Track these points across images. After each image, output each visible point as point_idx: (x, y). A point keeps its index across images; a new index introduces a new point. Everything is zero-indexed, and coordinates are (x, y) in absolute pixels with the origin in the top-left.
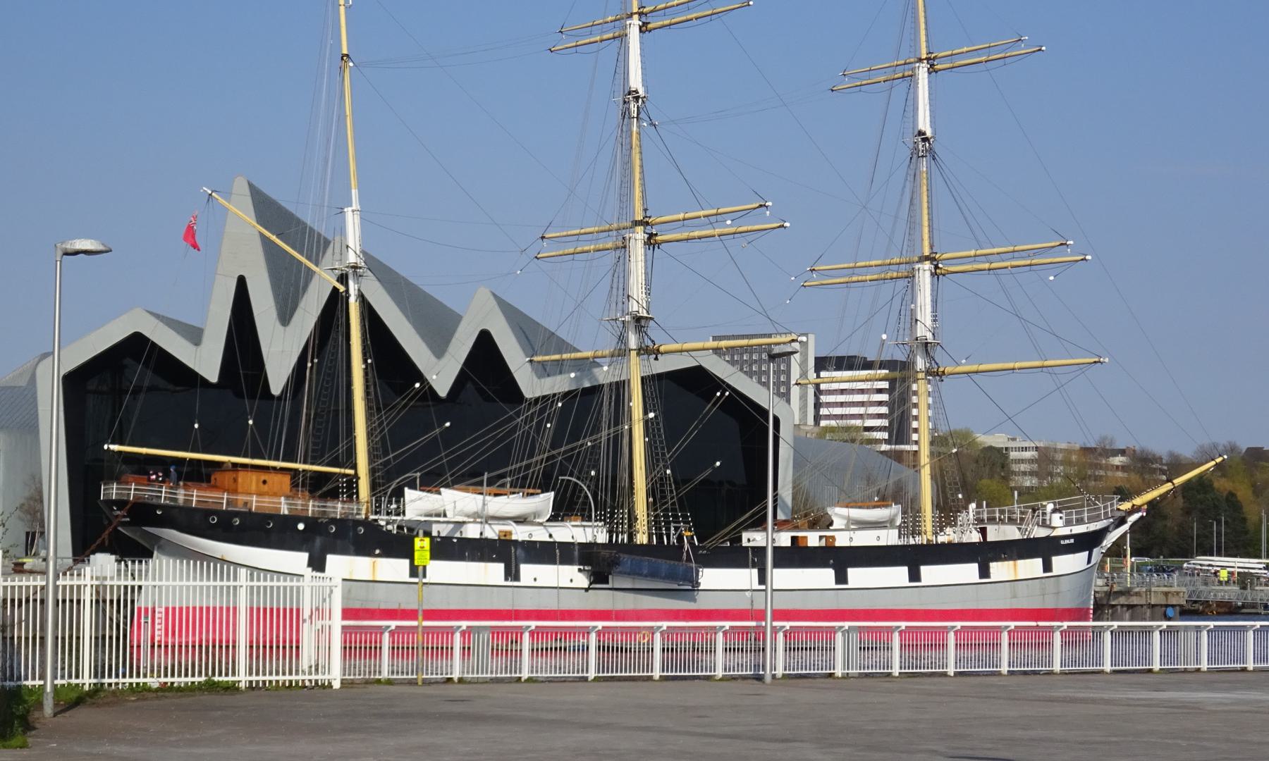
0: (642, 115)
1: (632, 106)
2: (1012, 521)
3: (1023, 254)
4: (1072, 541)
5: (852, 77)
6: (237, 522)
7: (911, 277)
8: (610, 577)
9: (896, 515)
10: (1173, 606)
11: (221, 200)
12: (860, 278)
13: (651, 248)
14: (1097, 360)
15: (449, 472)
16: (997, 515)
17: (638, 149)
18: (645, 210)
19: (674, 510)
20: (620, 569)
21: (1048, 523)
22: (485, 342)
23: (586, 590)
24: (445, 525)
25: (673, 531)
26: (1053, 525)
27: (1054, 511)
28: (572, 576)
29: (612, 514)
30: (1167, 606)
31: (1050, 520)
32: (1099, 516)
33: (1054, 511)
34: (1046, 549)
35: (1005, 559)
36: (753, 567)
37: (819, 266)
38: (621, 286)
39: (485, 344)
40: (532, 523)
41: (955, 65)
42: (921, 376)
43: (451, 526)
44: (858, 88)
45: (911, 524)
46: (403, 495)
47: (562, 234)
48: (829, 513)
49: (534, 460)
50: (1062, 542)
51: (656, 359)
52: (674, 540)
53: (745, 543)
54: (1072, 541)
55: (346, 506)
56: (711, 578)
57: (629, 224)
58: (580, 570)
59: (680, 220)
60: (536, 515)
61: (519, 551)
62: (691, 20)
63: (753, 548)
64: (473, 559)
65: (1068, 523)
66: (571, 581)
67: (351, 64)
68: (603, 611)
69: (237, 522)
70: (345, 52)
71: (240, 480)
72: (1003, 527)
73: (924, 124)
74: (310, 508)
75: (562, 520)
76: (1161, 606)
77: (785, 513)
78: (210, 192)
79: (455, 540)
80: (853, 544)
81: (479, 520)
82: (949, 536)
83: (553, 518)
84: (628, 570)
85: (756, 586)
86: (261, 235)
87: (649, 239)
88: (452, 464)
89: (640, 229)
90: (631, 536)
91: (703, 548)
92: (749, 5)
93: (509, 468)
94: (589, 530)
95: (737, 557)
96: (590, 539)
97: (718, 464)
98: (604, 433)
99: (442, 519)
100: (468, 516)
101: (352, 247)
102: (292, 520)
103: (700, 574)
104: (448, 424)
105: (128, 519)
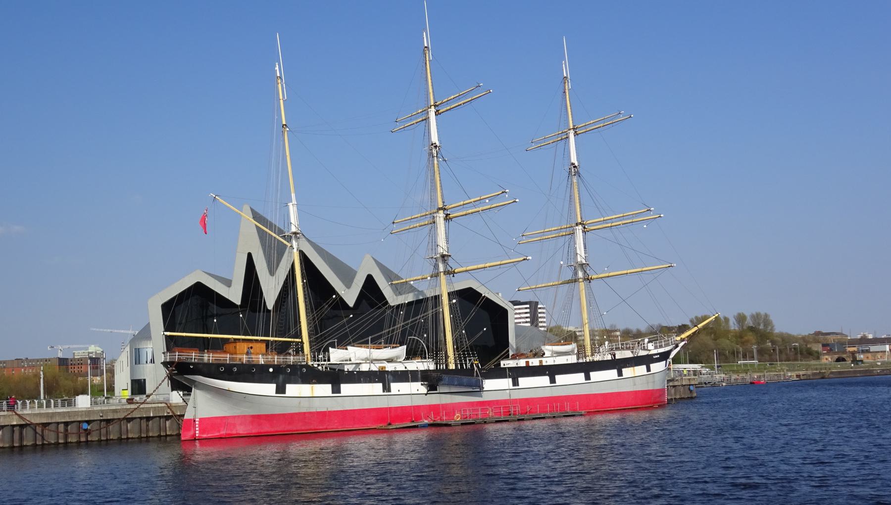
0: (439, 155)
1: (433, 151)
2: (628, 349)
3: (629, 217)
4: (658, 356)
5: (536, 143)
6: (235, 369)
7: (573, 234)
8: (438, 387)
9: (574, 348)
10: (693, 385)
11: (221, 200)
12: (547, 237)
13: (448, 221)
14: (670, 265)
15: (351, 335)
16: (620, 346)
17: (438, 173)
18: (444, 202)
19: (468, 351)
20: (443, 382)
21: (646, 348)
22: (370, 280)
23: (426, 394)
24: (351, 366)
25: (468, 362)
26: (649, 349)
27: (649, 342)
28: (418, 387)
29: (437, 354)
30: (690, 385)
31: (647, 347)
32: (668, 344)
33: (649, 342)
34: (647, 361)
35: (629, 367)
36: (510, 377)
37: (527, 233)
38: (434, 241)
39: (370, 281)
40: (396, 362)
41: (587, 130)
42: (580, 280)
43: (354, 366)
44: (539, 148)
45: (581, 351)
46: (328, 352)
47: (402, 220)
48: (543, 349)
49: (396, 327)
50: (654, 357)
51: (453, 276)
52: (469, 366)
53: (502, 366)
54: (658, 356)
55: (295, 358)
56: (490, 384)
57: (436, 210)
58: (422, 384)
59: (461, 205)
60: (398, 357)
61: (389, 376)
62: (461, 105)
63: (508, 368)
64: (365, 382)
65: (656, 348)
66: (418, 390)
67: (288, 129)
68: (435, 405)
69: (235, 369)
70: (284, 123)
71: (238, 347)
72: (623, 352)
73: (574, 159)
74: (276, 360)
75: (411, 359)
76: (687, 385)
77: (513, 351)
78: (214, 196)
79: (355, 373)
80: (555, 363)
81: (368, 362)
82: (597, 358)
83: (407, 359)
84: (447, 383)
85: (511, 387)
86: (257, 227)
87: (446, 216)
88: (352, 332)
89: (441, 212)
90: (447, 366)
91: (484, 369)
92: (490, 92)
93: (384, 332)
94: (425, 364)
95: (501, 373)
96: (426, 368)
97: (485, 329)
98: (430, 312)
99: (348, 362)
100: (363, 360)
101: (294, 223)
102: (266, 367)
103: (484, 382)
104: (351, 316)
105: (176, 372)
